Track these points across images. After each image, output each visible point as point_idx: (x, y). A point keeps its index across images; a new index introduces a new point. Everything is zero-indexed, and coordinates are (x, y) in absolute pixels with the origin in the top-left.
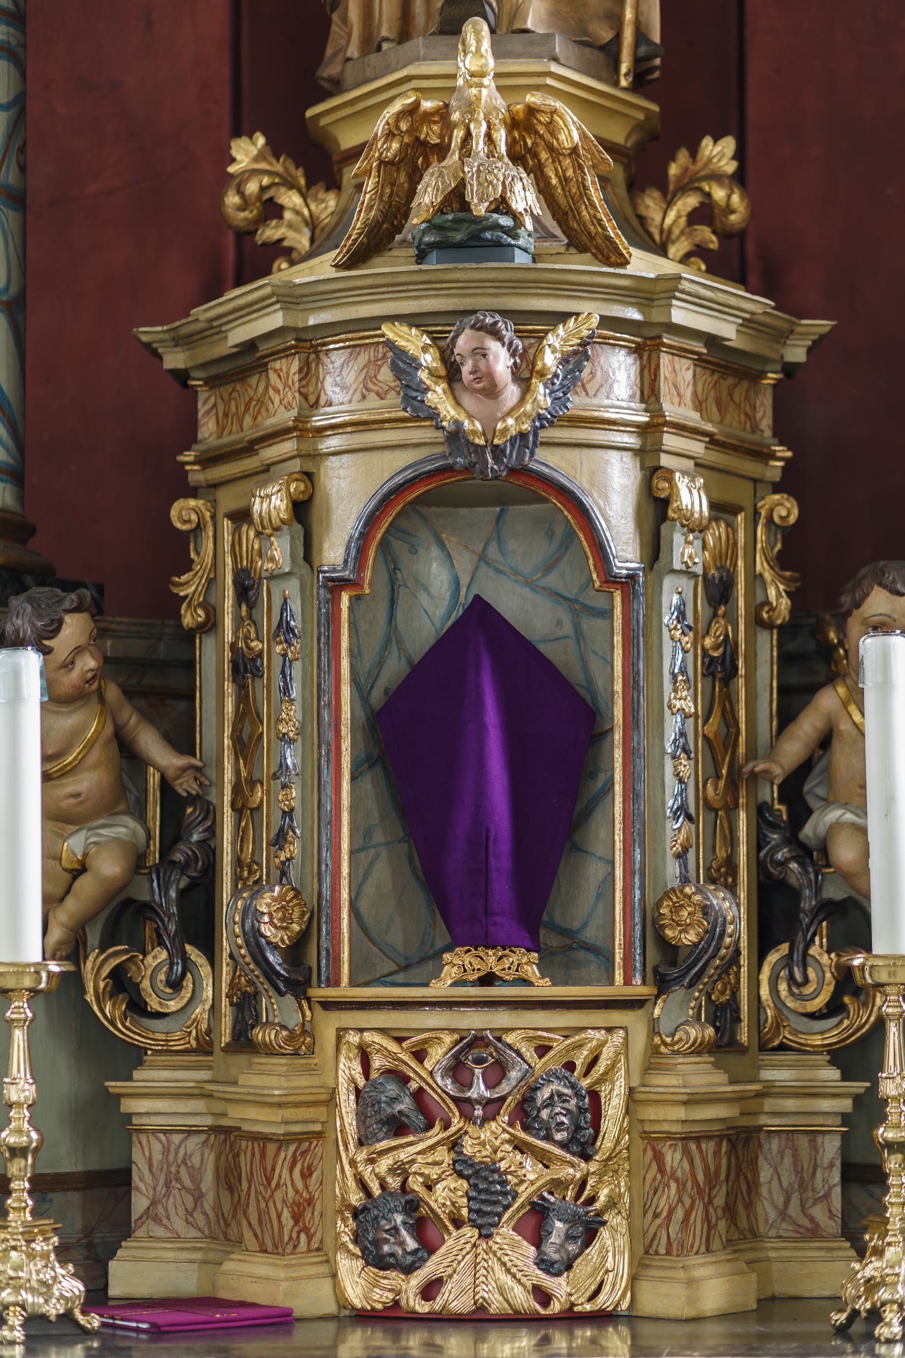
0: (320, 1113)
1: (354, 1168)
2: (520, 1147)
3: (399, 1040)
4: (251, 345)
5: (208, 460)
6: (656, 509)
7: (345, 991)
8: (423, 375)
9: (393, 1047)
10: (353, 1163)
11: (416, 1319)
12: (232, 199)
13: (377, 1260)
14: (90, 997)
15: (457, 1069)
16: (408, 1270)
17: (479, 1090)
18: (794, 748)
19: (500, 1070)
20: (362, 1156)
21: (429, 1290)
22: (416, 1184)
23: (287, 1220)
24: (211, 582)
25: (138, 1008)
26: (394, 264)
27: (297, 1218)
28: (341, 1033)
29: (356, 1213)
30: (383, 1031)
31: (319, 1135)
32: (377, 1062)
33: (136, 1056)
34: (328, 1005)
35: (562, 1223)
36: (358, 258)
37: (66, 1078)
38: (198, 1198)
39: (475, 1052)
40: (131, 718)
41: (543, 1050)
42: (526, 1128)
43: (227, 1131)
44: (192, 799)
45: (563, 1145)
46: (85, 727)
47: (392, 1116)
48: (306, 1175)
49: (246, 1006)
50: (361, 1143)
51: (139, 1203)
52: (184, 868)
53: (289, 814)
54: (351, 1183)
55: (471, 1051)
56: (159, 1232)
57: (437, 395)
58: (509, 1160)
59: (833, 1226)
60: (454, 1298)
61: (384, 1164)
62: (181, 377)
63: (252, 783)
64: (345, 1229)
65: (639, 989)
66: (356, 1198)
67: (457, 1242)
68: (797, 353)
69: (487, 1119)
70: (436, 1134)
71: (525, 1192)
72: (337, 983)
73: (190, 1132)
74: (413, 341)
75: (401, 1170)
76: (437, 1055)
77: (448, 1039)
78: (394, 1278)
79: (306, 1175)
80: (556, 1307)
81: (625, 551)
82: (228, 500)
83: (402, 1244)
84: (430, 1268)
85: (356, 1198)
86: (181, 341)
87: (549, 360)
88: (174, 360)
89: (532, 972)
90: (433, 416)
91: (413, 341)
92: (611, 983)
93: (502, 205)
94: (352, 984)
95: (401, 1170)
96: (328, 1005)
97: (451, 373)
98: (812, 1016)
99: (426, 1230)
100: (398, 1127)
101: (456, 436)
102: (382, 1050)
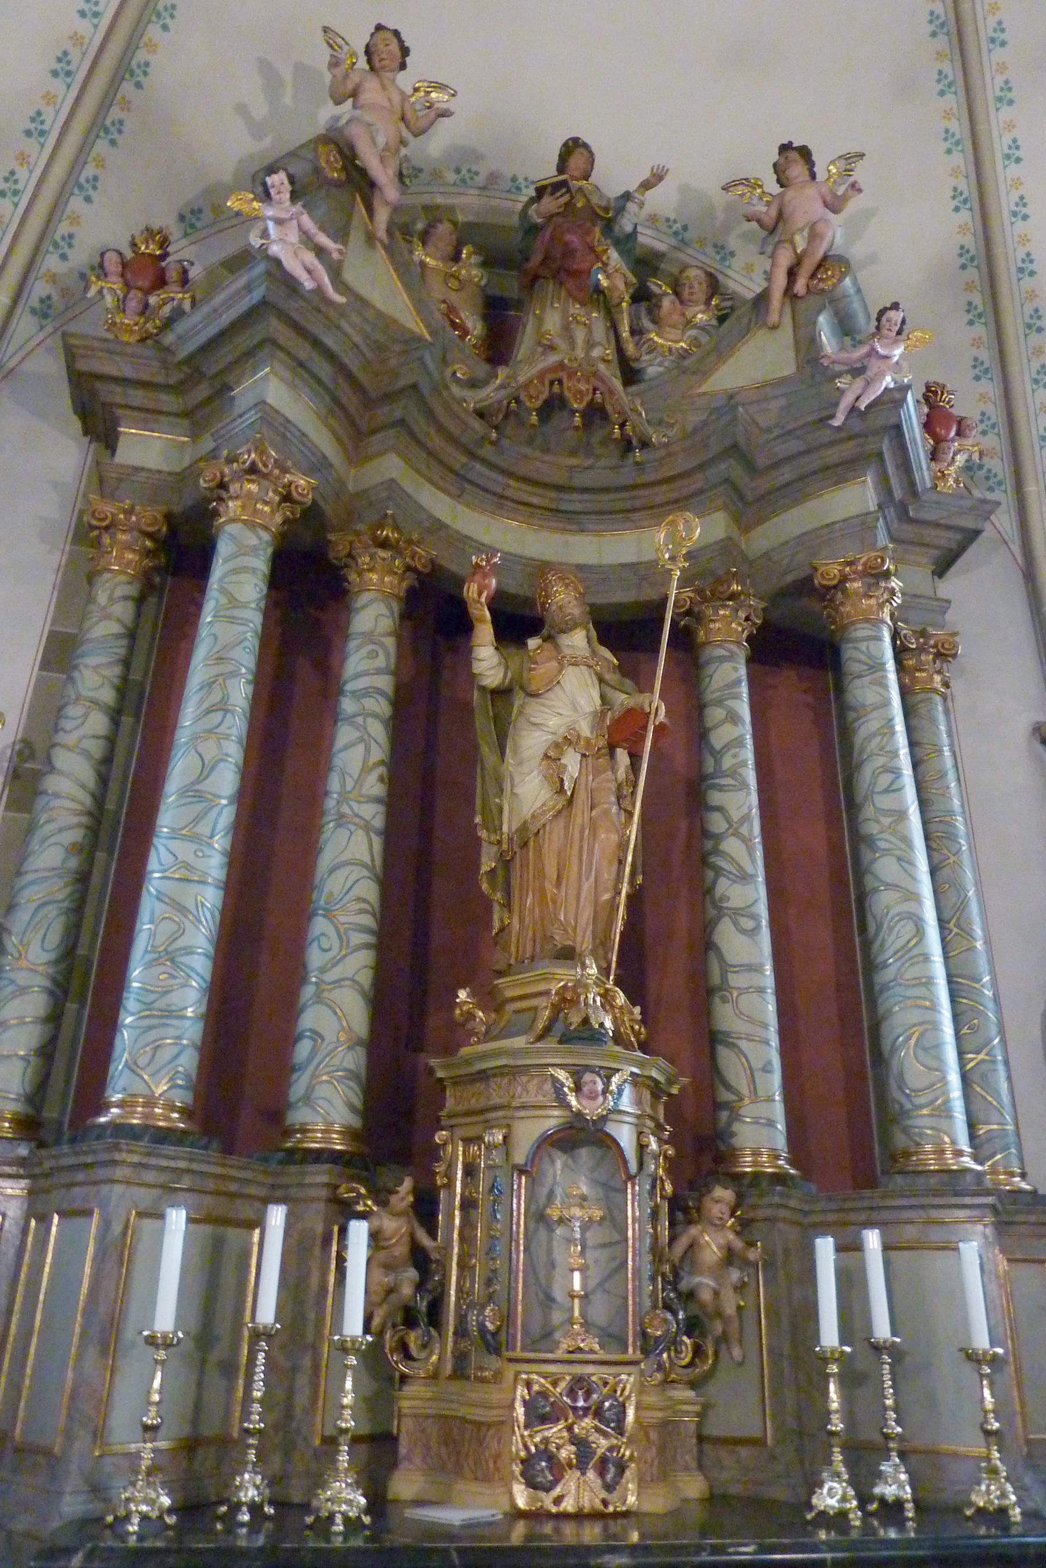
0: (505, 1412)
1: (521, 1440)
2: (597, 1430)
3: (545, 1378)
4: (484, 1071)
5: (450, 1116)
6: (642, 1148)
7: (518, 1353)
8: (566, 1089)
9: (542, 1381)
10: (522, 1436)
11: (550, 1516)
12: (458, 1012)
13: (531, 1484)
14: (387, 1351)
15: (572, 1393)
16: (548, 1490)
17: (581, 1403)
18: (679, 1248)
19: (588, 1394)
20: (526, 1433)
21: (558, 1501)
22: (552, 1448)
23: (491, 1465)
24: (450, 1166)
25: (408, 1356)
26: (551, 1043)
27: (495, 1463)
28: (517, 1374)
29: (523, 1462)
30: (537, 1373)
31: (502, 1423)
32: (536, 1388)
33: (404, 1378)
34: (511, 1360)
35: (612, 1469)
36: (540, 1038)
37: (370, 1386)
38: (429, 1449)
39: (580, 1385)
40: (416, 1224)
41: (606, 1384)
42: (600, 1421)
43: (446, 1417)
44: (437, 1261)
45: (613, 1429)
46: (400, 1229)
47: (540, 1414)
48: (499, 1442)
49: (461, 1358)
50: (526, 1427)
51: (403, 1450)
52: (430, 1292)
53: (495, 1271)
54: (521, 1446)
55: (580, 1384)
56: (411, 1466)
57: (572, 1100)
58: (594, 1437)
59: (693, 1464)
60: (568, 1505)
61: (537, 1439)
62: (441, 1080)
63: (470, 1257)
64: (517, 1469)
65: (639, 1355)
66: (523, 1454)
67: (571, 1478)
68: (675, 1091)
69: (585, 1415)
70: (561, 1425)
71: (600, 1452)
72: (514, 1349)
73: (428, 1416)
74: (562, 1075)
75: (546, 1441)
76: (563, 1385)
77: (568, 1378)
78: (542, 1494)
79: (499, 1442)
80: (611, 1509)
81: (633, 1167)
82: (460, 1132)
83: (545, 1477)
84: (557, 1491)
85: (523, 1454)
86: (446, 1067)
87: (613, 1087)
88: (440, 1074)
89: (597, 1347)
90: (569, 1106)
91: (562, 1075)
92: (626, 1351)
93: (602, 1025)
94: (523, 1349)
95: (546, 1441)
96: (511, 1360)
97: (578, 1089)
98: (684, 1367)
99: (558, 1469)
100: (545, 1419)
101: (579, 1115)
102: (538, 1382)
